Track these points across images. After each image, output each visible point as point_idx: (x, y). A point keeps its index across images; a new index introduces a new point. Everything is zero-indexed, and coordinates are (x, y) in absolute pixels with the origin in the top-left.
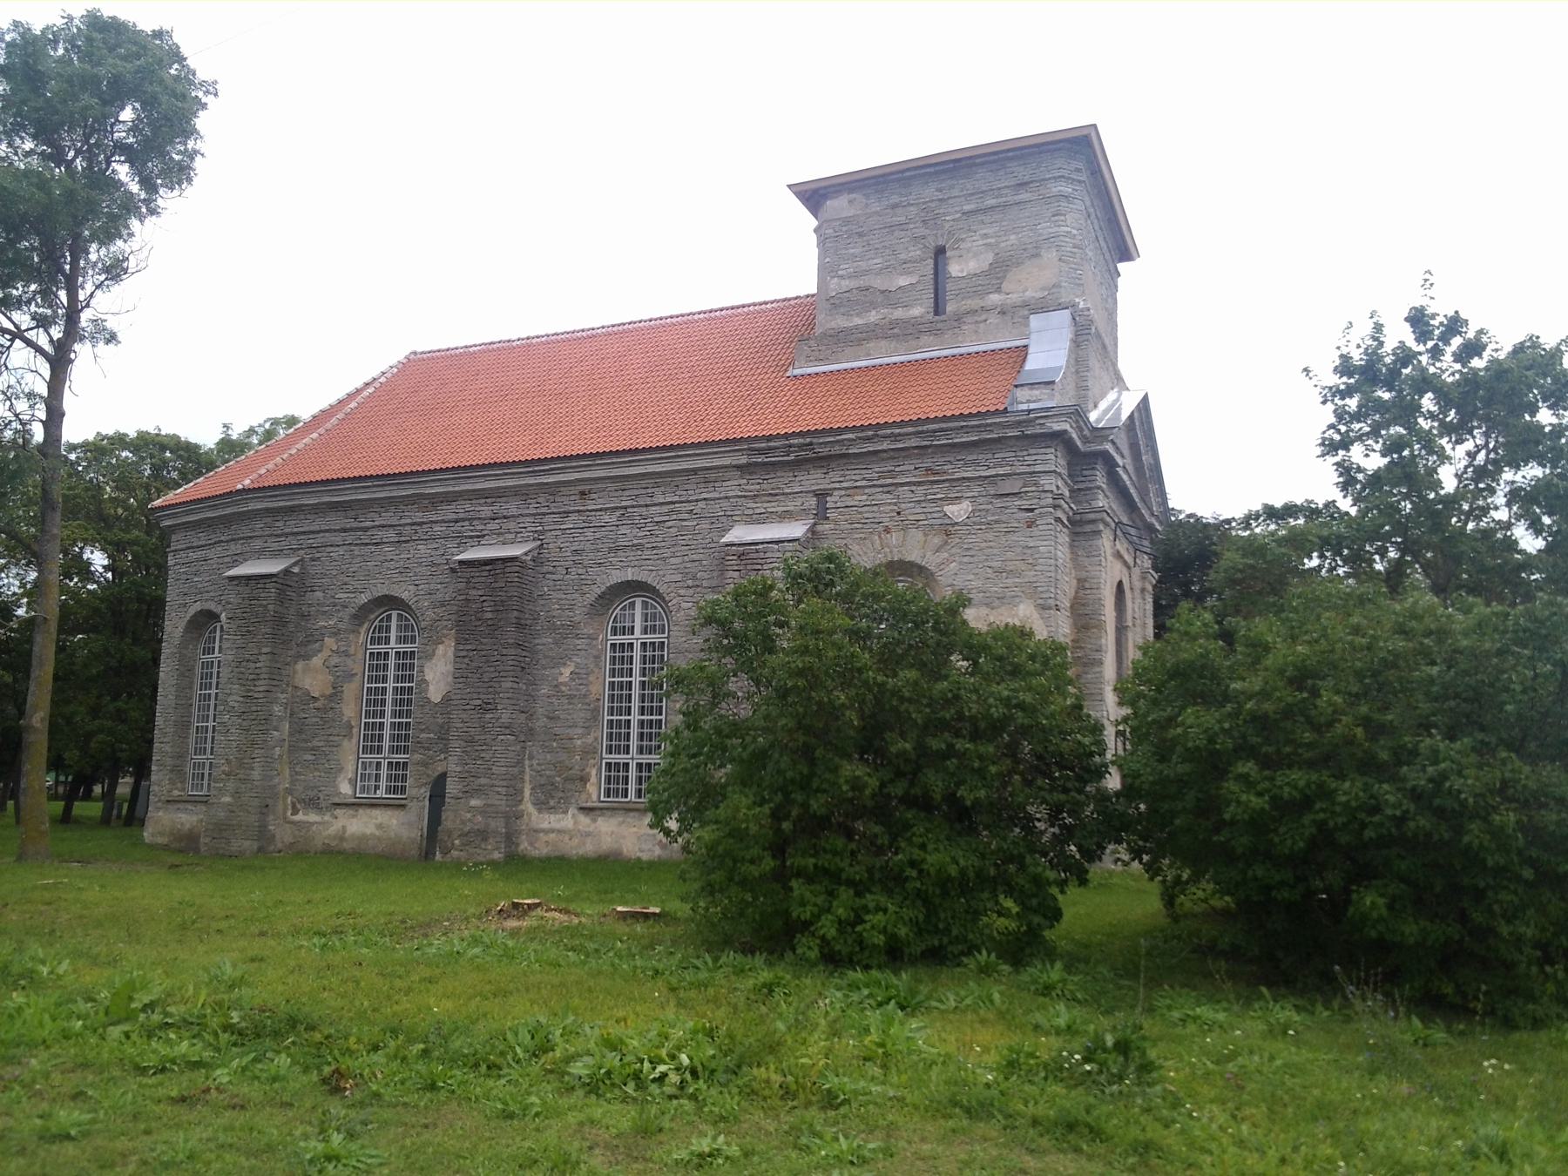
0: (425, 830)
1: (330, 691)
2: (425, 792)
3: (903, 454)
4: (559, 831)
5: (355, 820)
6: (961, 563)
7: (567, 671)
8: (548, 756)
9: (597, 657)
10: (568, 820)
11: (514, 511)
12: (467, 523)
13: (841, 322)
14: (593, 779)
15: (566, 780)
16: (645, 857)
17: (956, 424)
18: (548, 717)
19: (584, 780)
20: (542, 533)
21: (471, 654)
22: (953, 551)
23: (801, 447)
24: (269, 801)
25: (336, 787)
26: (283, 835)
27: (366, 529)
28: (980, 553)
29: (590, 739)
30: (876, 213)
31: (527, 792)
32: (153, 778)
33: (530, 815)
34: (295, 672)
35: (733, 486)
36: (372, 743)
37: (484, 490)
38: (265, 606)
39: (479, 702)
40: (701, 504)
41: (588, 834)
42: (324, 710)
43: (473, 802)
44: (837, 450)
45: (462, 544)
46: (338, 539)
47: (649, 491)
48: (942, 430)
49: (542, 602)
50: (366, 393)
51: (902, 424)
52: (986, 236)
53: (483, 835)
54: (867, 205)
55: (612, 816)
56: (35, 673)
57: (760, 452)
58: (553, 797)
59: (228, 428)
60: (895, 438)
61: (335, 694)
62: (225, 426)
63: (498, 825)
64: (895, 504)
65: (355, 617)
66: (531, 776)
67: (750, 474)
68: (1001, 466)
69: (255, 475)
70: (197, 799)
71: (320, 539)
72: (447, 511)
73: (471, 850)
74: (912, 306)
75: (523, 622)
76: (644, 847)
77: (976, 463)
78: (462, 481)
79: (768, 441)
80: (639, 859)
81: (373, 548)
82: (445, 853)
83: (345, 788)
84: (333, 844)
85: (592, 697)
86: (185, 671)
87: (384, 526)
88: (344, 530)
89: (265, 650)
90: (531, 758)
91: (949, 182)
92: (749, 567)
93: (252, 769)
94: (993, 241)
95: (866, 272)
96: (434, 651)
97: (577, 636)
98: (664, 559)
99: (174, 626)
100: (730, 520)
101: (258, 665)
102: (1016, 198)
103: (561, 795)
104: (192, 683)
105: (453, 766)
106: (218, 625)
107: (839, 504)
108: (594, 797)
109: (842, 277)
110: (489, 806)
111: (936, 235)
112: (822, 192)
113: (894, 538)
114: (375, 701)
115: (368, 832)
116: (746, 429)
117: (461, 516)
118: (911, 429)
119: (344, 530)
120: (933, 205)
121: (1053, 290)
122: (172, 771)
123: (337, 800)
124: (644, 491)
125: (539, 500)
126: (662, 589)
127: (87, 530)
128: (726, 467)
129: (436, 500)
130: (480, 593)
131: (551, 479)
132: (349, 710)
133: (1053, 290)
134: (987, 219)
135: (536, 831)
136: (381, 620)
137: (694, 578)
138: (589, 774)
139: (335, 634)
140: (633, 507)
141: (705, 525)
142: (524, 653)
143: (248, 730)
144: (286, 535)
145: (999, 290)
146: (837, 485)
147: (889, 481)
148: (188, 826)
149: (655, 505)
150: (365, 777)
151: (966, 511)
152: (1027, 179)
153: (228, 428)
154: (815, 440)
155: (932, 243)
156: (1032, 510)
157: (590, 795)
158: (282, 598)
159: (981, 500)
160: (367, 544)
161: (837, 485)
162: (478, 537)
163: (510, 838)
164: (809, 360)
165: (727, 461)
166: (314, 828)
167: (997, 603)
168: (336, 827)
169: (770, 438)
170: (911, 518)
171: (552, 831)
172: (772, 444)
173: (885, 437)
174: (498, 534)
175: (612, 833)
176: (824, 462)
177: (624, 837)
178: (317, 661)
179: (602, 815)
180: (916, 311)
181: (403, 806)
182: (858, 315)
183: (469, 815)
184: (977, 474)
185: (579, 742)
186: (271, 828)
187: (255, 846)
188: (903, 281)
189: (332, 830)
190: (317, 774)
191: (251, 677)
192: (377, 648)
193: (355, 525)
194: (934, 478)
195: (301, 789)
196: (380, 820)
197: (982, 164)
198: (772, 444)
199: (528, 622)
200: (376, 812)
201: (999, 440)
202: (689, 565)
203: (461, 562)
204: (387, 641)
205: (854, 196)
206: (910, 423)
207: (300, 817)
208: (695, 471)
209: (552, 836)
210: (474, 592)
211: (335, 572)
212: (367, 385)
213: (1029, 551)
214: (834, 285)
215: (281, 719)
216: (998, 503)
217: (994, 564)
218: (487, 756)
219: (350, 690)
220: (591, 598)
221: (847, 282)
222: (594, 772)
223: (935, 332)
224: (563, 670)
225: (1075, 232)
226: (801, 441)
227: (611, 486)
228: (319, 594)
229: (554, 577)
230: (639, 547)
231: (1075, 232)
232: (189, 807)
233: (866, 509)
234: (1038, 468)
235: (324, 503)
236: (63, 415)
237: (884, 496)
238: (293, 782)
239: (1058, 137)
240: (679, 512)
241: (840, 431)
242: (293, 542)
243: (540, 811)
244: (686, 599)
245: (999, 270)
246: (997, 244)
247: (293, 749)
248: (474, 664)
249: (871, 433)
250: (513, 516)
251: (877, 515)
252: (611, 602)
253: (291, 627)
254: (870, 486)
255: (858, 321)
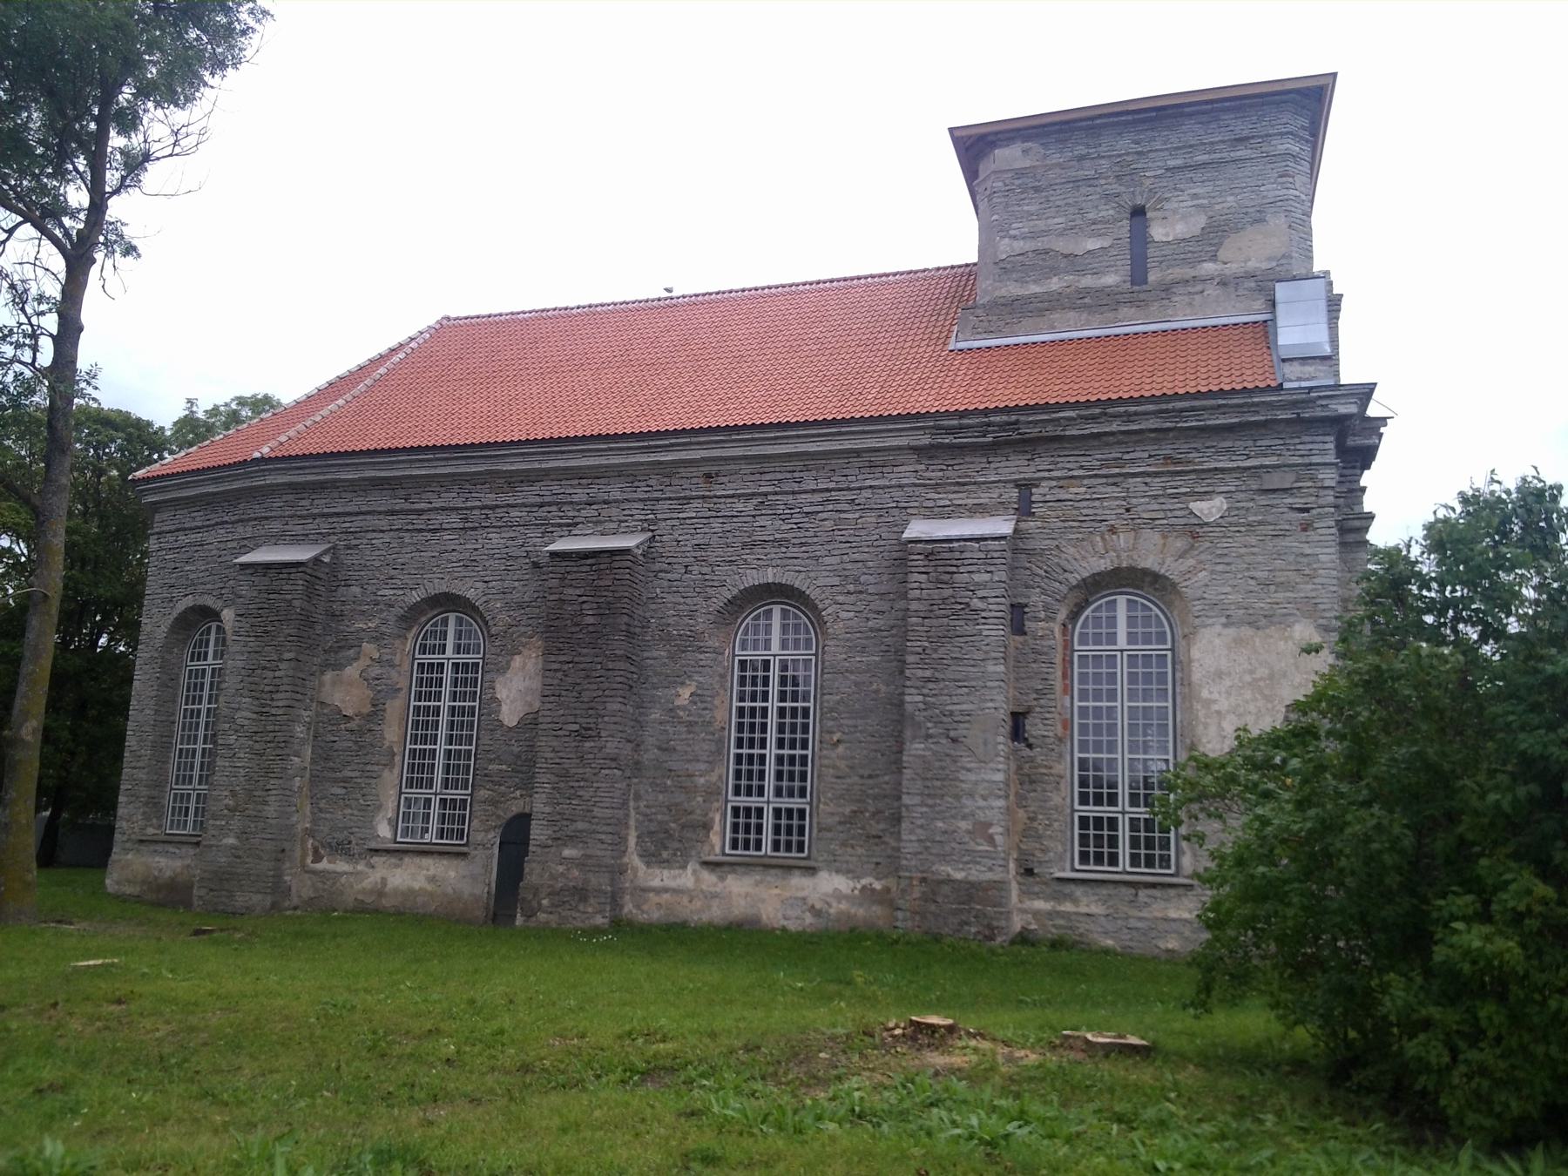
0: (493, 885)
1: (367, 709)
2: (494, 837)
3: (1135, 438)
4: (676, 891)
5: (399, 870)
6: (1212, 572)
7: (686, 692)
8: (661, 797)
9: (723, 676)
10: (686, 878)
11: (618, 496)
12: (554, 508)
13: (1013, 289)
14: (717, 827)
15: (683, 827)
16: (792, 926)
17: (1213, 402)
18: (660, 748)
19: (707, 827)
20: (655, 522)
21: (565, 667)
22: (1203, 557)
23: (1003, 426)
24: (287, 845)
25: (373, 828)
26: (301, 887)
27: (420, 512)
28: (1239, 561)
29: (714, 778)
30: (1059, 165)
31: (632, 841)
32: (121, 811)
33: (635, 870)
34: (321, 684)
35: (906, 473)
36: (419, 774)
37: (579, 468)
38: (290, 601)
39: (576, 727)
40: (866, 494)
41: (715, 896)
42: (360, 732)
43: (567, 852)
44: (1050, 430)
45: (548, 533)
46: (383, 523)
47: (796, 475)
48: (1193, 409)
49: (653, 606)
50: (395, 359)
51: (1141, 400)
52: (1195, 196)
53: (581, 893)
54: (1045, 156)
55: (745, 874)
56: (27, 668)
57: (949, 430)
58: (666, 848)
59: (192, 404)
60: (1129, 417)
61: (375, 713)
62: (189, 401)
63: (600, 881)
64: (1124, 499)
65: (402, 618)
66: (637, 820)
67: (930, 458)
68: (1265, 456)
69: (273, 443)
70: (183, 839)
71: (359, 522)
72: (529, 494)
73: (564, 914)
74: (1104, 273)
75: (632, 630)
76: (790, 913)
77: (1228, 450)
78: (553, 456)
79: (961, 417)
80: (784, 929)
81: (429, 536)
82: (529, 915)
83: (384, 831)
84: (368, 900)
85: (717, 725)
86: (168, 682)
87: (443, 509)
88: (392, 513)
89: (287, 656)
90: (638, 797)
91: (1149, 133)
92: (941, 569)
93: (266, 803)
94: (1205, 201)
95: (1046, 233)
96: (508, 663)
97: (700, 650)
98: (817, 558)
99: (155, 623)
100: (906, 513)
101: (277, 674)
102: (1232, 154)
103: (676, 845)
104: (175, 695)
105: (539, 805)
106: (214, 625)
107: (1048, 498)
108: (718, 850)
109: (1014, 237)
110: (590, 857)
111: (1133, 192)
112: (991, 138)
113: (1123, 540)
114: (424, 724)
115: (416, 886)
116: (924, 402)
117: (547, 499)
118: (1151, 407)
119: (392, 513)
120: (1129, 158)
121: (1283, 261)
122: (146, 804)
123: (373, 845)
124: (789, 475)
125: (650, 483)
126: (814, 594)
127: (18, 513)
128: (899, 448)
129: (514, 480)
130: (578, 592)
131: (670, 457)
132: (391, 733)
133: (1283, 261)
134: (1197, 176)
135: (645, 890)
136: (435, 625)
137: (856, 581)
138: (712, 820)
139: (376, 639)
140: (776, 493)
141: (871, 518)
142: (633, 669)
143: (261, 755)
144: (314, 517)
145: (1214, 258)
146: (1046, 474)
147: (1117, 470)
148: (168, 873)
149: (806, 492)
150: (407, 818)
151: (1219, 510)
152: (1245, 133)
153: (192, 404)
154: (1022, 418)
155: (1128, 201)
156: (1307, 510)
157: (713, 847)
158: (310, 594)
159: (1241, 496)
160: (420, 531)
161: (1046, 474)
162: (569, 525)
163: (615, 899)
164: (976, 332)
165: (903, 441)
166: (343, 880)
167: (1263, 622)
168: (373, 878)
169: (965, 414)
170: (1145, 515)
171: (666, 890)
172: (965, 421)
173: (1115, 416)
174: (596, 523)
175: (747, 895)
176: (1029, 445)
177: (763, 901)
178: (352, 671)
179: (734, 872)
180: (1110, 280)
181: (464, 855)
182: (1035, 282)
183: (561, 869)
184: (1235, 465)
185: (702, 780)
186: (287, 878)
187: (268, 901)
188: (1092, 244)
189: (367, 884)
190: (349, 811)
191: (268, 688)
192: (428, 658)
193: (407, 506)
194: (1175, 468)
195: (326, 830)
196: (431, 872)
197: (1191, 115)
198: (965, 421)
199: (638, 630)
200: (427, 861)
201: (1265, 424)
202: (849, 566)
203: (554, 554)
204: (443, 649)
205: (1029, 144)
206: (1153, 399)
207: (324, 865)
208: (857, 453)
209: (666, 896)
210: (570, 591)
211: (377, 564)
212: (393, 351)
213: (1305, 560)
214: (1005, 247)
215: (303, 742)
216: (1263, 500)
217: (1258, 574)
218: (586, 794)
219: (394, 708)
220: (716, 603)
221: (1022, 243)
222: (717, 818)
223: (1138, 303)
224: (681, 691)
225: (1303, 197)
226: (1005, 418)
227: (746, 468)
228: (356, 590)
229: (669, 576)
230: (779, 543)
231: (1303, 197)
232: (171, 849)
233: (1085, 504)
234: (1315, 459)
235: (364, 479)
236: (81, 329)
237: (1109, 489)
238: (314, 821)
239: (1289, 86)
240: (837, 502)
241: (1059, 407)
242: (324, 526)
243: (648, 864)
244: (845, 607)
245: (1215, 234)
246: (1211, 206)
247: (315, 780)
248: (569, 680)
249: (1098, 411)
250: (616, 501)
251: (1099, 511)
252: (741, 608)
253: (319, 629)
254: (1090, 477)
255: (1035, 289)
